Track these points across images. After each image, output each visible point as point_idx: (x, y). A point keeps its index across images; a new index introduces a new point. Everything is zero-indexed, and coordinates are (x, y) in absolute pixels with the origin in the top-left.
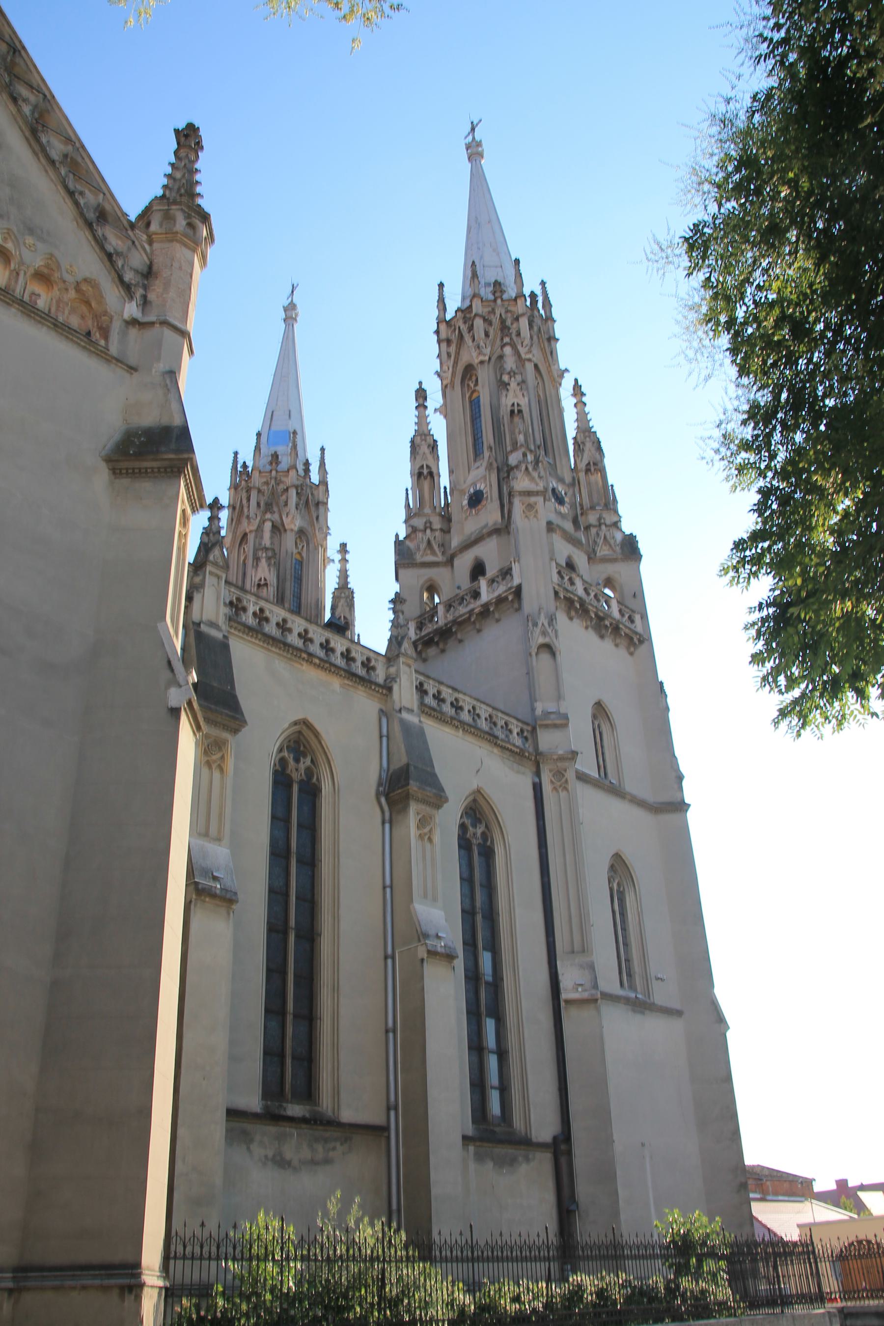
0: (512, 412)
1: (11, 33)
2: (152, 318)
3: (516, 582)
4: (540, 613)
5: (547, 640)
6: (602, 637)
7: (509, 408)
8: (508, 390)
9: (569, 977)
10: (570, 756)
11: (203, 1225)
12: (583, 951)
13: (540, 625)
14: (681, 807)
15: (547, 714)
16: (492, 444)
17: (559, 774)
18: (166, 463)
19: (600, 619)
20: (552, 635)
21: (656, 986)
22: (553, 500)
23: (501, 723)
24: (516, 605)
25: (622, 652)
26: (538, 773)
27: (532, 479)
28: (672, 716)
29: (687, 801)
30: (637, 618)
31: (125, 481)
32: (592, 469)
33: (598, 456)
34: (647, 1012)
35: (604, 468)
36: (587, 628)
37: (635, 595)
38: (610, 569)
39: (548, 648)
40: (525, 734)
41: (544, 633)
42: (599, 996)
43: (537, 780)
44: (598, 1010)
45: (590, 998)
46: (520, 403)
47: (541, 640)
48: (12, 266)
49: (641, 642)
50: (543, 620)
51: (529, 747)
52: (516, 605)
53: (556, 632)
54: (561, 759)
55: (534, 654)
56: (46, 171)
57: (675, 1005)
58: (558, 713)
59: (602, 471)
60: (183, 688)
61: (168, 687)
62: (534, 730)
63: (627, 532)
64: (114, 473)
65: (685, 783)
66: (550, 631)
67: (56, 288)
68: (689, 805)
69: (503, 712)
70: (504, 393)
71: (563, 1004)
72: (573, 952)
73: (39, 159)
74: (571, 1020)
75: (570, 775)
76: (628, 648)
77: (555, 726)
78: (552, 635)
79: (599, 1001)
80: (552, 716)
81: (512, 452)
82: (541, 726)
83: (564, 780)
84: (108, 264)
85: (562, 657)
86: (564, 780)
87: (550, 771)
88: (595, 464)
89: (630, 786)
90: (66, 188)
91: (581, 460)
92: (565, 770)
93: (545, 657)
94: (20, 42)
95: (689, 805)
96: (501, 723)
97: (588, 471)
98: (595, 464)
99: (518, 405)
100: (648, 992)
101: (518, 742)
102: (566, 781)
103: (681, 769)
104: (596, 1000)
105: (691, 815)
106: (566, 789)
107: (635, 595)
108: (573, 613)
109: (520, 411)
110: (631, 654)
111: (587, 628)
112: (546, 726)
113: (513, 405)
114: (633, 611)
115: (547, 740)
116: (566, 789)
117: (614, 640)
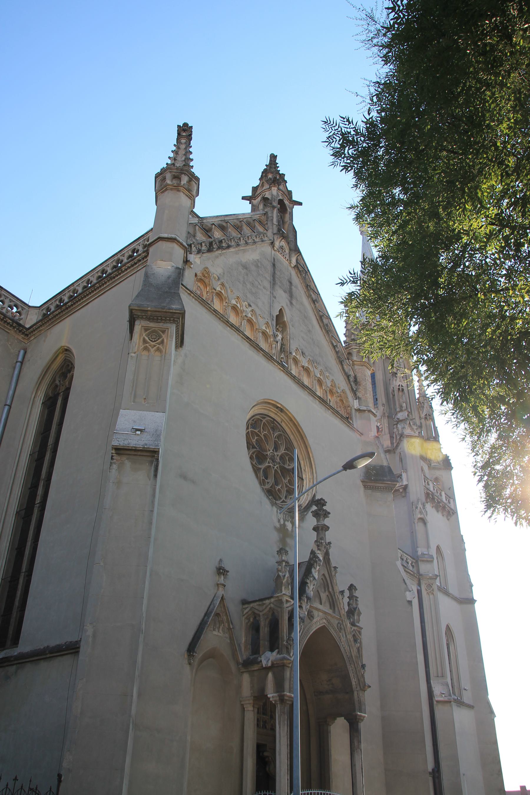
0: (399, 389)
1: (303, 263)
2: (365, 408)
3: (405, 483)
4: (418, 502)
5: (422, 516)
6: (438, 511)
7: (398, 387)
8: (396, 377)
9: (437, 689)
10: (435, 577)
11: (16, 779)
12: (443, 677)
13: (419, 508)
14: (471, 601)
15: (423, 554)
16: (384, 402)
17: (429, 586)
18: (386, 485)
19: (439, 502)
20: (425, 514)
21: (464, 692)
22: (507, 492)
23: (405, 559)
24: (403, 495)
25: (445, 518)
26: (419, 584)
27: (412, 429)
28: (468, 554)
29: (475, 598)
30: (451, 501)
31: (369, 491)
32: (428, 418)
33: (431, 411)
34: (461, 706)
35: (434, 417)
36: (432, 507)
37: (449, 489)
38: (438, 473)
39: (423, 521)
40: (413, 564)
41: (421, 513)
42: (452, 700)
43: (419, 588)
44: (451, 706)
45: (448, 700)
46: (403, 385)
47: (419, 516)
48: (323, 387)
49: (453, 514)
50: (420, 506)
51: (415, 570)
52: (403, 495)
53: (426, 512)
54: (431, 578)
55: (416, 523)
56: (325, 336)
57: (470, 702)
58: (428, 554)
59: (433, 420)
60: (411, 592)
61: (405, 591)
62: (417, 562)
63: (444, 453)
64: (365, 487)
65: (473, 588)
66: (423, 512)
67: (334, 396)
68: (476, 601)
69: (406, 553)
70: (395, 379)
71: (435, 703)
72: (438, 676)
73: (322, 330)
74: (439, 710)
75: (435, 587)
76: (447, 517)
77: (427, 561)
78: (425, 514)
79: (452, 702)
80: (426, 556)
81: (400, 412)
82: (421, 560)
83: (432, 589)
84: (347, 381)
85: (429, 525)
86: (432, 589)
87: (425, 584)
88: (429, 415)
89: (451, 591)
90: (332, 344)
91: (423, 412)
92: (432, 584)
93: (421, 524)
94: (307, 268)
95: (476, 601)
96: (405, 559)
97: (426, 418)
98: (429, 415)
99: (402, 386)
100: (461, 695)
101: (411, 568)
102: (433, 590)
103: (472, 581)
104: (450, 702)
105: (476, 605)
106: (433, 594)
107: (449, 489)
108: (428, 500)
109: (403, 390)
110: (448, 520)
111: (432, 507)
112: (423, 561)
113: (399, 386)
114: (450, 498)
115: (424, 568)
116: (433, 594)
117: (442, 513)
